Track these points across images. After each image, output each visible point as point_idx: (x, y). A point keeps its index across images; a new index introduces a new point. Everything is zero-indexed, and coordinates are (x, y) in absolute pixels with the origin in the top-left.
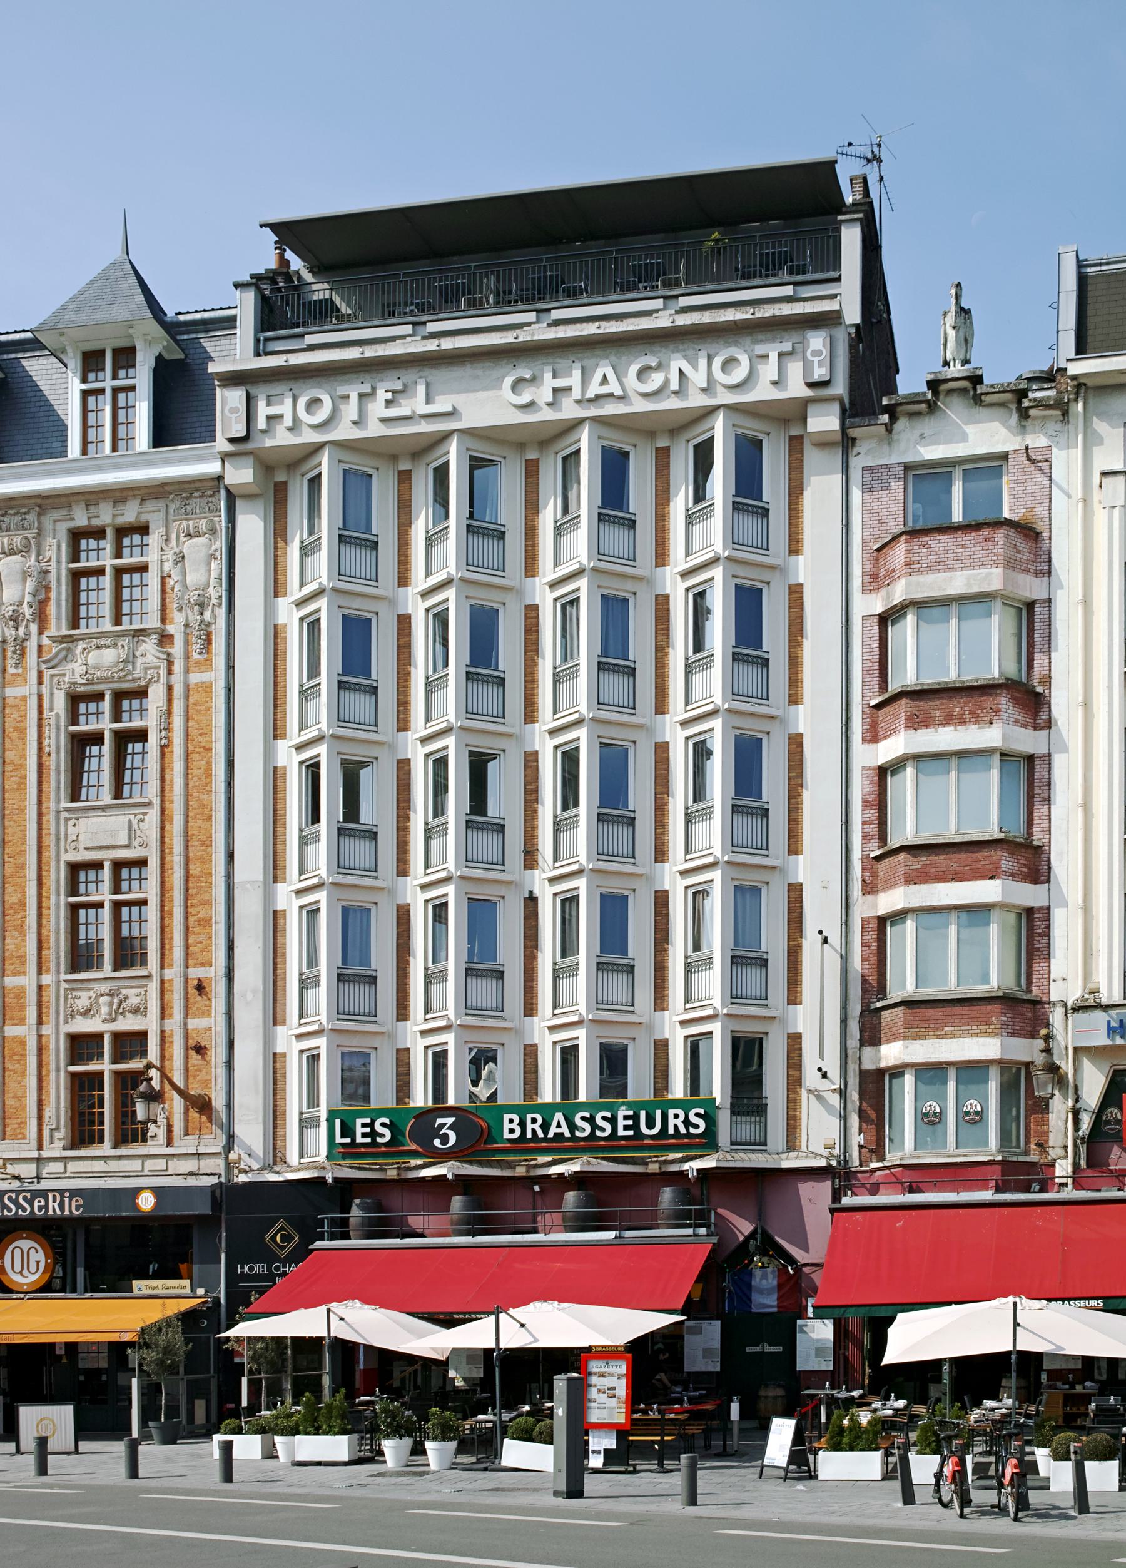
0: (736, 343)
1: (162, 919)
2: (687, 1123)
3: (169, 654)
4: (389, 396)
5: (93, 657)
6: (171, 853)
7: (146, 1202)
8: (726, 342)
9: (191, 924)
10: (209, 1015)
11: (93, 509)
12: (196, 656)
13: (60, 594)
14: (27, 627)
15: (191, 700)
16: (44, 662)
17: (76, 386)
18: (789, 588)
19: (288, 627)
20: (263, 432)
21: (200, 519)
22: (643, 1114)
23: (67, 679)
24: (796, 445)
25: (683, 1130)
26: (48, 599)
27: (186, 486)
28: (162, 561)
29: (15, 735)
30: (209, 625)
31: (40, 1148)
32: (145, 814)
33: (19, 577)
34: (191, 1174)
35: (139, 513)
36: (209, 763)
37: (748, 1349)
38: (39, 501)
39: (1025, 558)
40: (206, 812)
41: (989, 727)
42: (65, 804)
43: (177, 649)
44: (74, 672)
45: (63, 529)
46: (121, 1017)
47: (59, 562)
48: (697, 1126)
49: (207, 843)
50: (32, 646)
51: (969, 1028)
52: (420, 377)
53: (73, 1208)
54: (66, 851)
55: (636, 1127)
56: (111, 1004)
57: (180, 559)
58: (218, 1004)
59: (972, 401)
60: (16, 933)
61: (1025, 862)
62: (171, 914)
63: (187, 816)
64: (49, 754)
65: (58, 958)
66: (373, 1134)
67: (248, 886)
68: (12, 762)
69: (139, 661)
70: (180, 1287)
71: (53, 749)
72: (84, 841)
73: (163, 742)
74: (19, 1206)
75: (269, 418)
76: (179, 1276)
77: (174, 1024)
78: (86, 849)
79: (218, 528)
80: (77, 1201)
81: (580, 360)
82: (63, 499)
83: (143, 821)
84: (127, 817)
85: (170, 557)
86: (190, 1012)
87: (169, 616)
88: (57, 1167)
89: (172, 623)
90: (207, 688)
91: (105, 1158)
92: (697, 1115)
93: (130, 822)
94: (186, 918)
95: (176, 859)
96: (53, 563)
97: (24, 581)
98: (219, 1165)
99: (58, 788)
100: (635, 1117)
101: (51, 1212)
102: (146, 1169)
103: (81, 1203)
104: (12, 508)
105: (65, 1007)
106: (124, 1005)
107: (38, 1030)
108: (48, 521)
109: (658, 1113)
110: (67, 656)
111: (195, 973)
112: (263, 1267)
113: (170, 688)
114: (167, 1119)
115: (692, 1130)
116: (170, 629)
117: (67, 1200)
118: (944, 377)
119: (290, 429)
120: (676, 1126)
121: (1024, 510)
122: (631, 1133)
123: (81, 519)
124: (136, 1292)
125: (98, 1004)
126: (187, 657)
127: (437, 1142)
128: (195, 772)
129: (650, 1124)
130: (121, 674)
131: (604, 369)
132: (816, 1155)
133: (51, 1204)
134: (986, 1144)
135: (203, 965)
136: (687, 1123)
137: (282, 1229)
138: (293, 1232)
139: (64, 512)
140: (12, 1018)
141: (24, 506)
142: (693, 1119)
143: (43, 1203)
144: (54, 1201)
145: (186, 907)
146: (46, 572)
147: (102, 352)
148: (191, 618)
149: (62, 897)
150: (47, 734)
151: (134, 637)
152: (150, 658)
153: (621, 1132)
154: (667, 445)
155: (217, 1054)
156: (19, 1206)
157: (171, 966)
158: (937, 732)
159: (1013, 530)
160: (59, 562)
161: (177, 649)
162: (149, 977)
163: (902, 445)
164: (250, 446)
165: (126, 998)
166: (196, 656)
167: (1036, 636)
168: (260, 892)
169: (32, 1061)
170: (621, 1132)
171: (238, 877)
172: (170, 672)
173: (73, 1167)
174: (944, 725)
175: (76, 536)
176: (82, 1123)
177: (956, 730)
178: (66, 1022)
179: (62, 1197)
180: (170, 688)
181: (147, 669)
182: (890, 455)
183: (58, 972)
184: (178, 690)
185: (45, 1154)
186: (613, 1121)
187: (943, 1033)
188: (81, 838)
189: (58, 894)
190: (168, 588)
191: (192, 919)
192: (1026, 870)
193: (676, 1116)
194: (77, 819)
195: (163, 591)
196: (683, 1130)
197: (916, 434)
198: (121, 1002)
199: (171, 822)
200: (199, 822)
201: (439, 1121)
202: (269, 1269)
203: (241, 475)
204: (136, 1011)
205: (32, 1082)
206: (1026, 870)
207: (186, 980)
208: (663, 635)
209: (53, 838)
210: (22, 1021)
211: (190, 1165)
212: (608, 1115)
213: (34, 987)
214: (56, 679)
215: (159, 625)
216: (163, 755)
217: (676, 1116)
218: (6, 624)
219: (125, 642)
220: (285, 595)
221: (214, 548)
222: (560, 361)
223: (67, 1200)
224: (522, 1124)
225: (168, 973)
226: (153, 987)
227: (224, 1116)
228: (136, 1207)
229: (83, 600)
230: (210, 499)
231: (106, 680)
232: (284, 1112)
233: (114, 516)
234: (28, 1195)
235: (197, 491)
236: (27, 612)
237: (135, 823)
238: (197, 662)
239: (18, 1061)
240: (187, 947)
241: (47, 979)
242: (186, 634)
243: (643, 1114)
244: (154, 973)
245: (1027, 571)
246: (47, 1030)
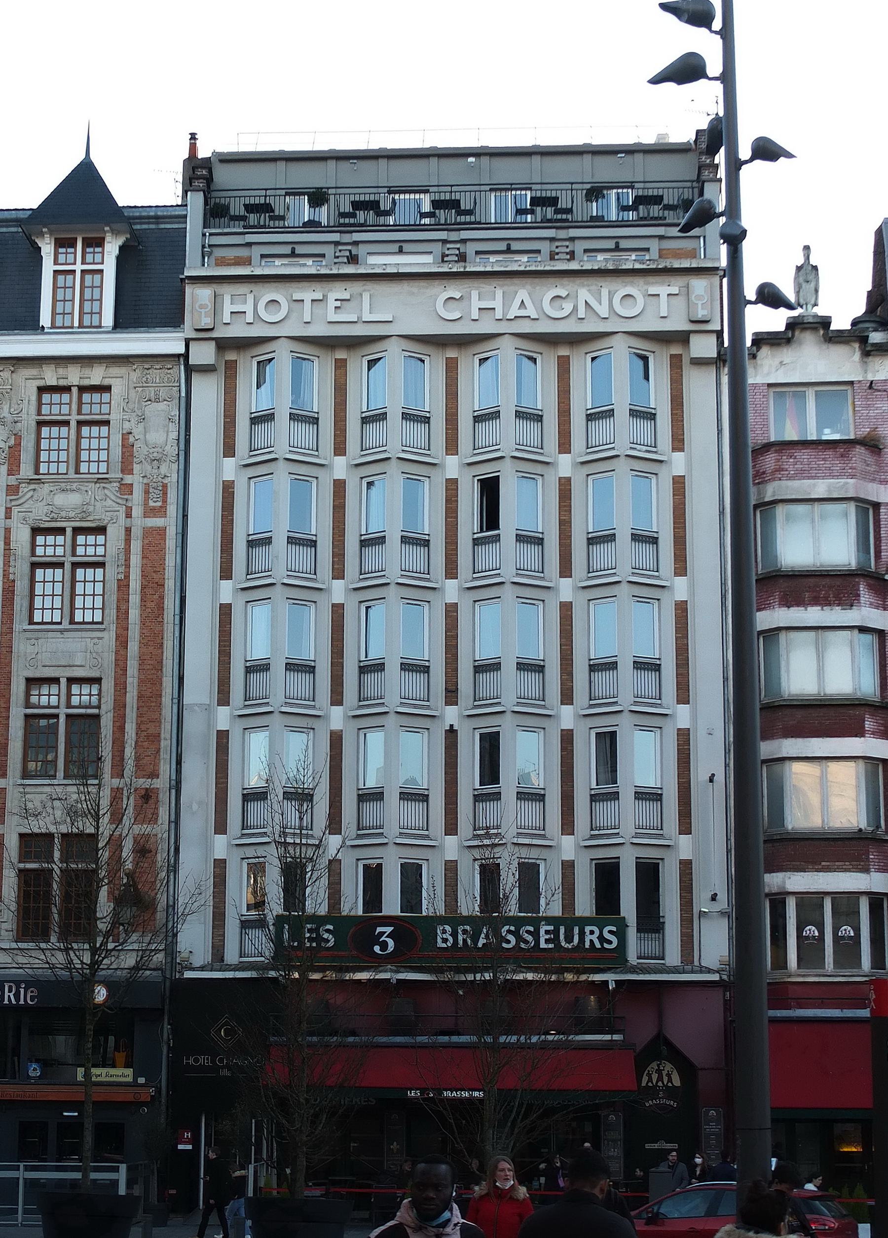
0: (632, 284)
2: (601, 938)
4: (338, 304)
5: (60, 500)
8: (623, 282)
13: (28, 443)
18: (673, 479)
22: (562, 930)
24: (676, 363)
25: (598, 945)
36: (162, 598)
37: (647, 1146)
39: (872, 469)
41: (851, 609)
45: (34, 385)
48: (610, 942)
51: (843, 863)
52: (364, 290)
55: (555, 940)
59: (822, 339)
61: (882, 722)
66: (319, 939)
67: (196, 708)
80: (32, 992)
81: (502, 286)
92: (610, 932)
100: (556, 932)
109: (576, 930)
112: (208, 1059)
113: (128, 531)
115: (606, 946)
117: (22, 991)
118: (801, 321)
120: (591, 941)
121: (868, 430)
122: (551, 946)
123: (51, 377)
127: (377, 949)
129: (569, 939)
131: (523, 294)
132: (709, 971)
134: (859, 965)
136: (601, 938)
142: (607, 935)
144: (10, 991)
151: (96, 483)
153: (543, 945)
154: (568, 354)
158: (806, 610)
159: (863, 448)
163: (765, 369)
167: (882, 532)
170: (543, 945)
171: (187, 700)
172: (129, 515)
174: (812, 605)
177: (822, 610)
180: (128, 531)
182: (756, 376)
186: (536, 935)
187: (820, 867)
192: (882, 728)
193: (592, 932)
194: (37, 639)
196: (598, 945)
197: (777, 361)
200: (151, 648)
201: (379, 929)
202: (213, 1061)
203: (202, 354)
206: (882, 728)
208: (566, 511)
212: (531, 929)
217: (592, 932)
222: (484, 286)
223: (22, 991)
224: (454, 934)
230: (169, 371)
231: (68, 519)
243: (562, 930)
245: (873, 480)
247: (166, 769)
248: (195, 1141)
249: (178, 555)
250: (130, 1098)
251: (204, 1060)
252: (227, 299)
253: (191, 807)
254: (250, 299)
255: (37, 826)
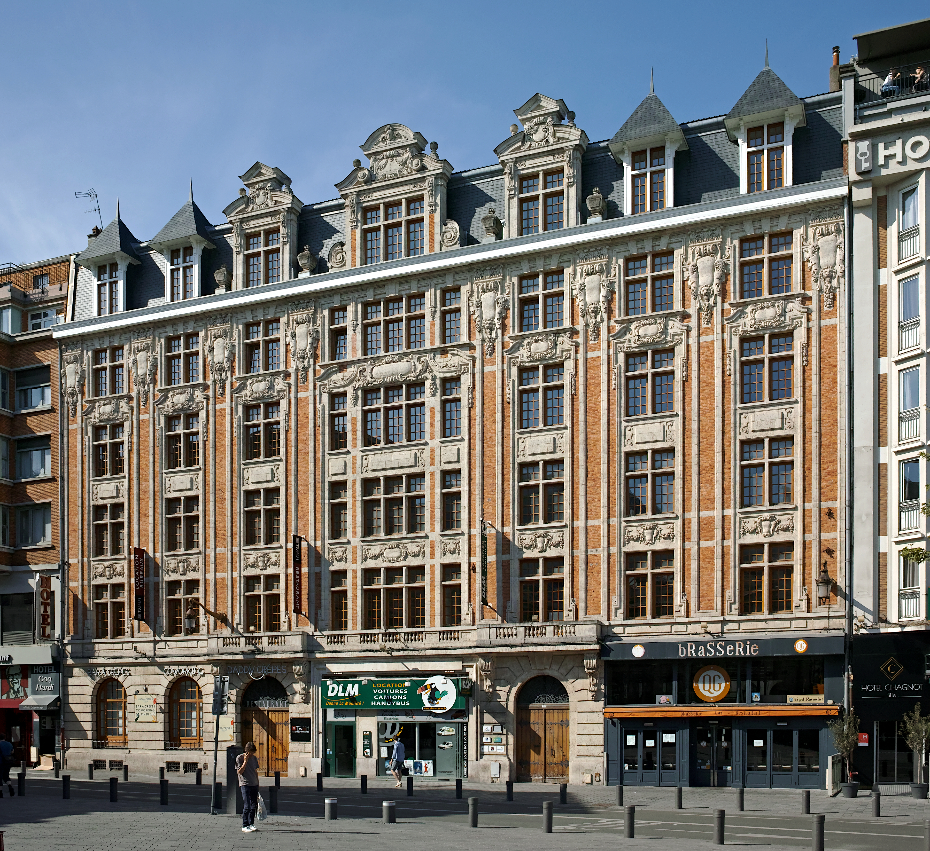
1: (804, 472)
3: (808, 309)
6: (810, 431)
7: (801, 647)
9: (823, 475)
10: (836, 531)
11: (254, 313)
12: (826, 309)
14: (715, 298)
15: (822, 336)
16: (726, 320)
17: (744, 149)
19: (888, 288)
20: (882, 166)
21: (829, 224)
23: (740, 329)
26: (727, 280)
27: (820, 205)
28: (572, 290)
29: (706, 365)
30: (835, 288)
31: (723, 615)
32: (792, 408)
33: (710, 269)
34: (825, 629)
35: (788, 224)
36: (835, 375)
38: (723, 222)
40: (833, 405)
42: (739, 405)
43: (814, 305)
44: (168, 407)
46: (775, 533)
47: (735, 258)
49: (834, 423)
50: (717, 312)
53: (752, 651)
54: (625, 445)
56: (184, 566)
57: (294, 336)
58: (841, 523)
60: (707, 485)
62: (810, 469)
63: (820, 408)
64: (729, 375)
65: (735, 499)
68: (705, 381)
69: (670, 331)
70: (818, 699)
71: (321, 424)
72: (751, 427)
73: (805, 363)
74: (716, 650)
75: (886, 157)
76: (817, 693)
77: (812, 537)
78: (754, 431)
79: (841, 228)
82: (739, 220)
83: (790, 412)
84: (780, 411)
85: (810, 249)
86: (822, 529)
87: (807, 285)
88: (735, 626)
89: (578, 324)
90: (833, 328)
91: (766, 620)
93: (782, 413)
94: (820, 471)
95: (814, 435)
96: (732, 259)
97: (713, 271)
98: (842, 623)
99: (735, 395)
101: (737, 654)
102: (674, 630)
103: (757, 648)
104: (705, 227)
105: (740, 528)
106: (778, 526)
107: (723, 543)
108: (157, 332)
110: (741, 314)
111: (826, 504)
114: (576, 606)
116: (809, 293)
117: (748, 646)
119: (899, 163)
124: (788, 701)
125: (761, 526)
126: (699, 326)
128: (825, 380)
130: (778, 323)
133: (737, 649)
135: (831, 499)
137: (892, 663)
138: (899, 664)
139: (737, 227)
140: (705, 537)
141: (713, 226)
143: (732, 648)
144: (740, 647)
145: (820, 464)
146: (728, 264)
147: (762, 127)
148: (824, 286)
149: (738, 462)
150: (728, 362)
152: (795, 313)
155: (840, 555)
156: (716, 650)
157: (810, 501)
160: (735, 258)
161: (814, 305)
162: (565, 526)
164: (871, 176)
165: (780, 521)
166: (488, 357)
168: (871, 453)
169: (718, 562)
171: (856, 445)
172: (576, 352)
173: (743, 626)
175: (248, 326)
176: (370, 616)
178: (740, 537)
179: (745, 644)
180: (809, 330)
181: (793, 319)
183: (735, 507)
184: (815, 331)
185: (727, 618)
188: (635, 436)
189: (735, 460)
190: (807, 269)
191: (823, 472)
195: (804, 271)
198: (776, 525)
199: (811, 412)
200: (829, 411)
204: (787, 529)
205: (718, 574)
207: (820, 509)
209: (732, 426)
210: (712, 538)
211: (823, 623)
213: (720, 517)
214: (733, 329)
215: (468, 342)
216: (572, 398)
218: (702, 298)
219: (188, 390)
220: (885, 266)
221: (839, 241)
223: (748, 646)
225: (808, 506)
226: (798, 514)
227: (230, 621)
228: (794, 649)
229: (391, 335)
232: (886, 590)
233: (375, 295)
234: (723, 644)
235: (827, 206)
236: (716, 290)
237: (785, 414)
238: (827, 313)
239: (709, 562)
240: (820, 489)
241: (728, 512)
242: (699, 314)
244: (799, 506)
246: (728, 543)
247: (842, 493)
248: (871, 741)
249: (622, 300)
250: (824, 713)
251: (876, 687)
252: (881, 146)
253: (861, 518)
254: (899, 142)
255: (371, 564)
